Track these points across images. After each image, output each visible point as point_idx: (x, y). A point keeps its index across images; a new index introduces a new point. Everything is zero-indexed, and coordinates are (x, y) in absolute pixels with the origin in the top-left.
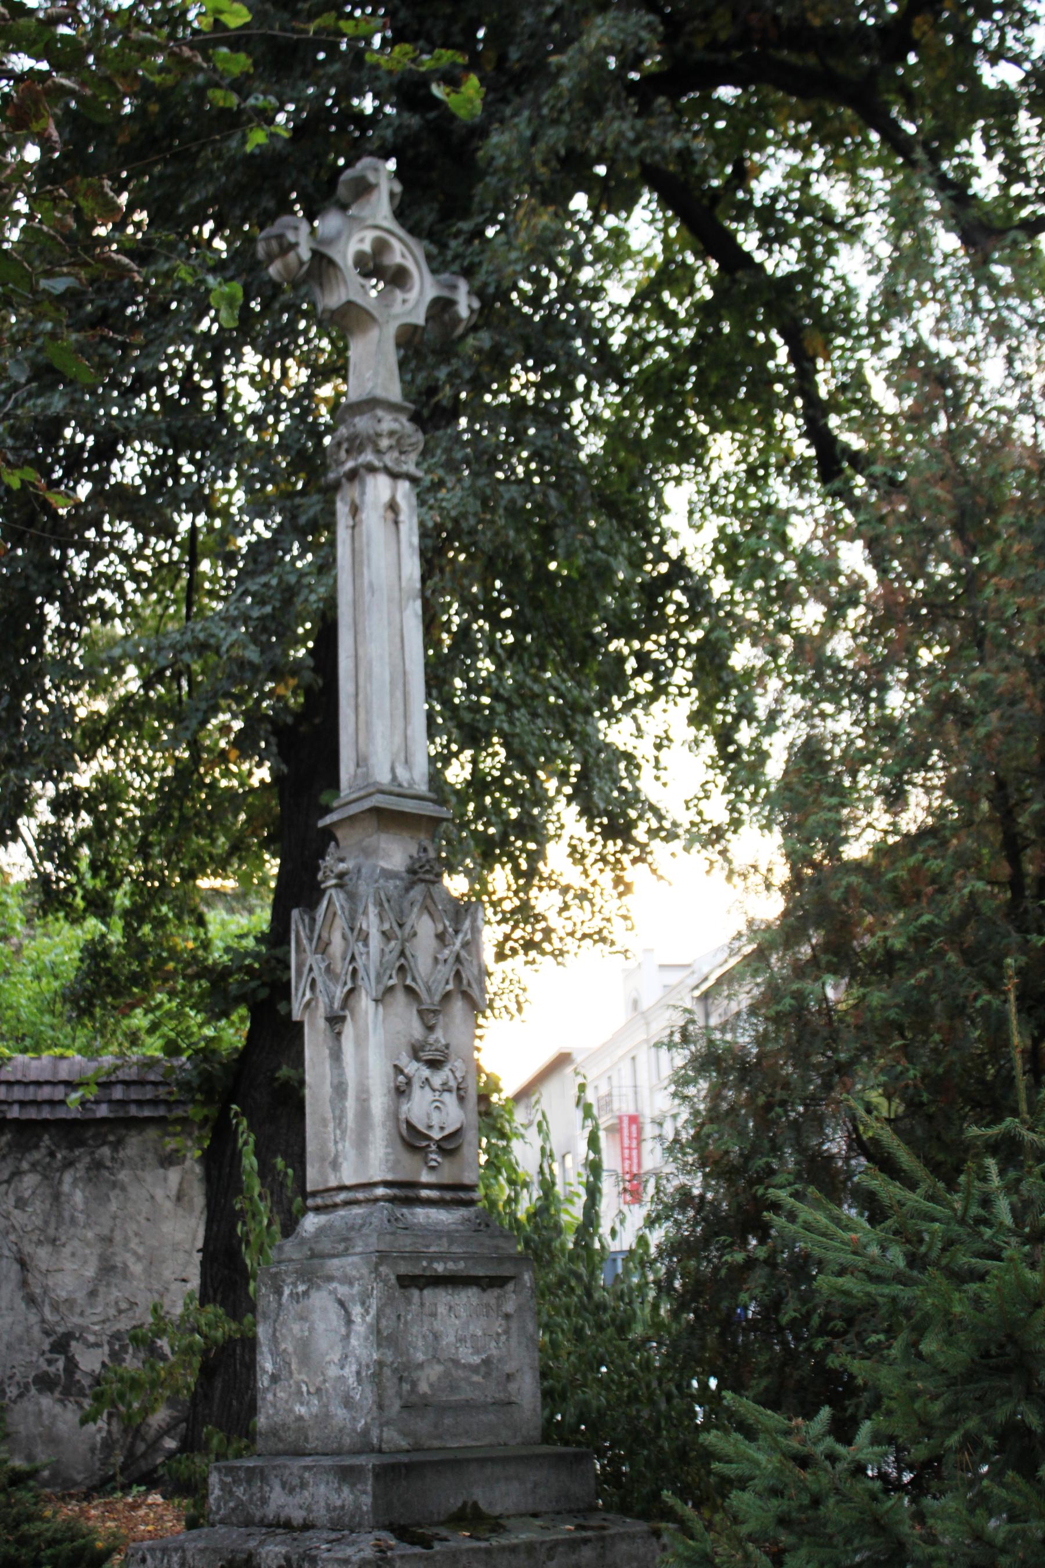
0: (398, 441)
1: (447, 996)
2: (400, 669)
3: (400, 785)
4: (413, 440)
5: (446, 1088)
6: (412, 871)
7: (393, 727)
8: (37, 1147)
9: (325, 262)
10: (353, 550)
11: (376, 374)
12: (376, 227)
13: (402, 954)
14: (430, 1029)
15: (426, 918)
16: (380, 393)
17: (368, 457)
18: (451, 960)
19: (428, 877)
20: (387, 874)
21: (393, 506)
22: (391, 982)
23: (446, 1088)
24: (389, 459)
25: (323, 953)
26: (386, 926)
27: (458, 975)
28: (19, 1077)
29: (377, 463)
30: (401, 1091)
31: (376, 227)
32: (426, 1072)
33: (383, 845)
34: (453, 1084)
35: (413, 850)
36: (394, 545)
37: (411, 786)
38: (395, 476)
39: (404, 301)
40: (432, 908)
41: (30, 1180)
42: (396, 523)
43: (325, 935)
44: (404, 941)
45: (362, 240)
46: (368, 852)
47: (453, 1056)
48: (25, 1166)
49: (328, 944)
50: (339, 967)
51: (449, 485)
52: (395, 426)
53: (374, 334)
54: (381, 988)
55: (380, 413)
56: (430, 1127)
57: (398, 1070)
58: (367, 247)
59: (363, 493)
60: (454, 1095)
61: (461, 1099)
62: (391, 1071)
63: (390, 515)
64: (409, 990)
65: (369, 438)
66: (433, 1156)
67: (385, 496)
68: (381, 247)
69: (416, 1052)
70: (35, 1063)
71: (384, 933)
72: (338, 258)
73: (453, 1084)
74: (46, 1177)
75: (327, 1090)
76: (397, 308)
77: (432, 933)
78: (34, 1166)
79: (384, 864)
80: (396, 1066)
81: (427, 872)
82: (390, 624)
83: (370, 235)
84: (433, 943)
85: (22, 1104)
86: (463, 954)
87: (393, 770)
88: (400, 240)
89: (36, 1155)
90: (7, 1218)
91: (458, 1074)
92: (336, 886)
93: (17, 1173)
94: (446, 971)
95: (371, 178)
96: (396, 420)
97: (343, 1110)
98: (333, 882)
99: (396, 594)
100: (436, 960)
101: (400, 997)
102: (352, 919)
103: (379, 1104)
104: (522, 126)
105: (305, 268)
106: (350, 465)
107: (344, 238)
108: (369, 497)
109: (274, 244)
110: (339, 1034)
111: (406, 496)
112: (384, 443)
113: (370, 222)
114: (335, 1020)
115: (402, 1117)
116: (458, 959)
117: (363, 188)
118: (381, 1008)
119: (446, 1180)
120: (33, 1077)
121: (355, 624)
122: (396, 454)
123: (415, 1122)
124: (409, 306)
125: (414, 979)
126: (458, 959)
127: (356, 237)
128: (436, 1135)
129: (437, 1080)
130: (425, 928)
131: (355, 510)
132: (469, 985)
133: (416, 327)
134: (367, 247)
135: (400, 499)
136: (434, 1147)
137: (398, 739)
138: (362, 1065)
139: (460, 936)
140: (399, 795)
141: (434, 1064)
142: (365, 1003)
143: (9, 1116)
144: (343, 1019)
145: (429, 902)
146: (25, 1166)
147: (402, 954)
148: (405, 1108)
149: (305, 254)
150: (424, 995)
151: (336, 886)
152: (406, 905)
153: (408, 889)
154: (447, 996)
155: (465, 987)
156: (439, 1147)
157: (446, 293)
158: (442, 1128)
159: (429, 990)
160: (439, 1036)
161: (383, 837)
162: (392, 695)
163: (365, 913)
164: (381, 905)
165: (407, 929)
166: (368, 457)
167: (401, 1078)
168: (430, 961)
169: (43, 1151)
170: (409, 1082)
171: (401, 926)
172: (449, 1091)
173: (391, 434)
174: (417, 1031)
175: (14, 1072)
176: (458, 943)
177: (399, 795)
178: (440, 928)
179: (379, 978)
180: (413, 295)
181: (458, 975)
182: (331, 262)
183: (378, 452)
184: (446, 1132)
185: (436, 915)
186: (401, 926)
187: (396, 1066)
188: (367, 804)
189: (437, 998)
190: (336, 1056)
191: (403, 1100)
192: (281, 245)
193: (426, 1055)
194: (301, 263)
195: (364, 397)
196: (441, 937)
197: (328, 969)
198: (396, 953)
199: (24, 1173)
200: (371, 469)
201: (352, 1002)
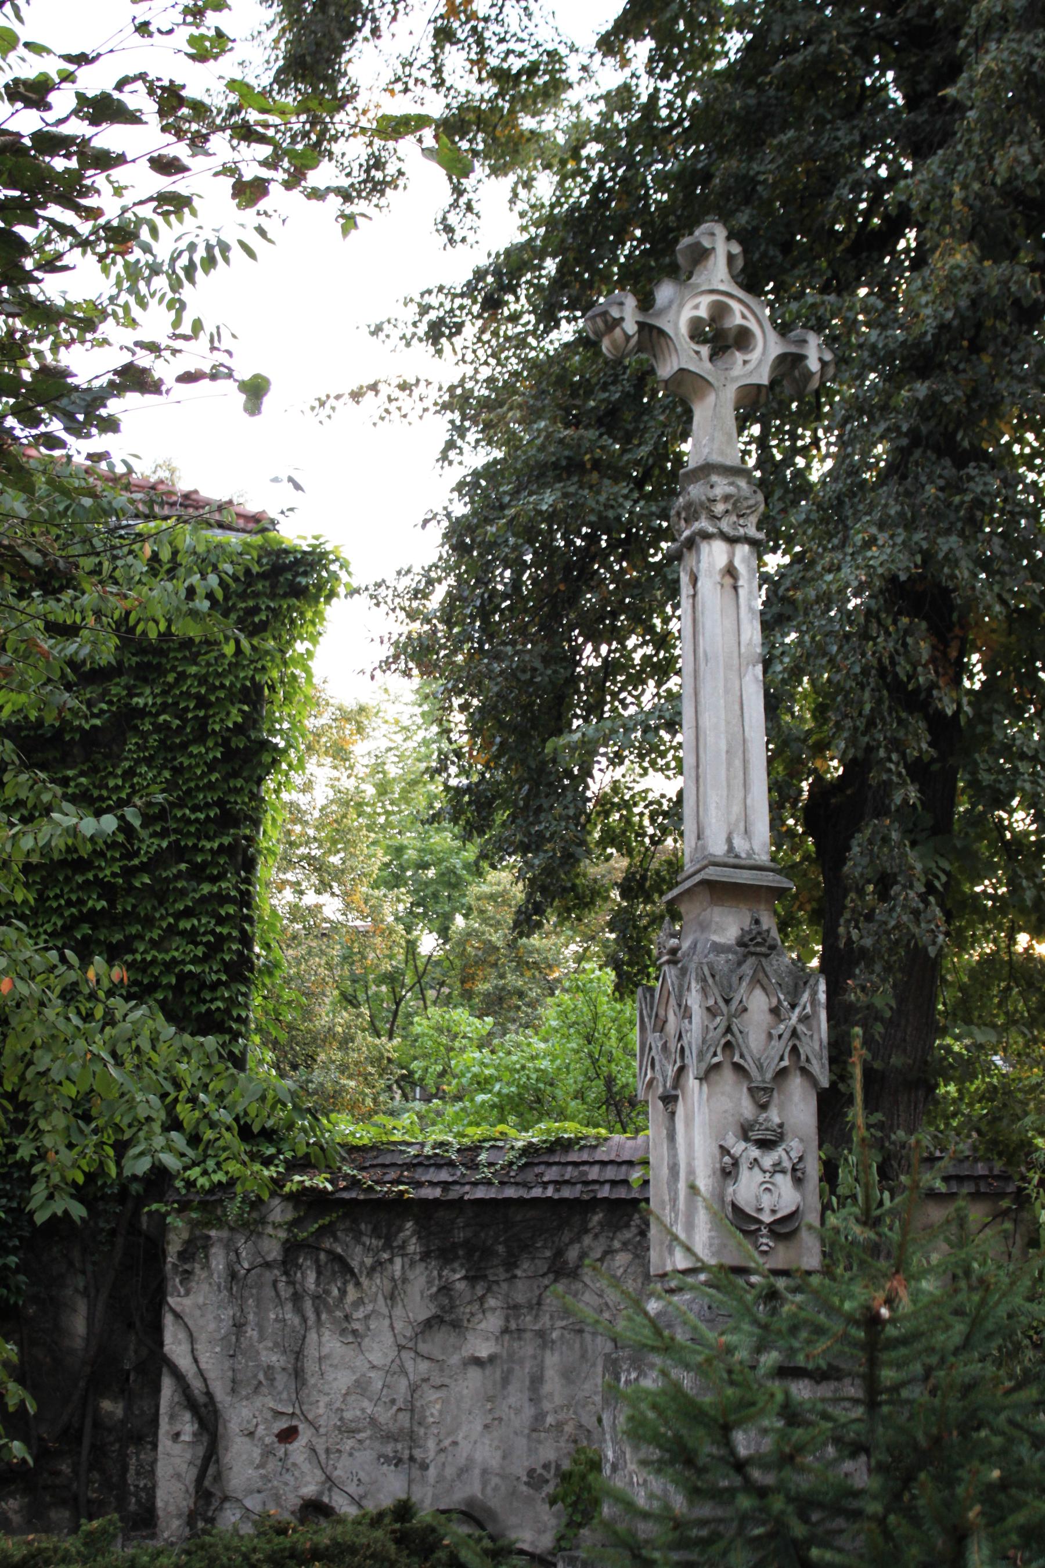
0: (734, 504)
1: (782, 1074)
2: (740, 737)
3: (737, 856)
4: (751, 502)
5: (778, 1168)
6: (741, 943)
7: (729, 797)
8: (627, 1226)
9: (655, 333)
10: (695, 621)
11: (712, 439)
12: (712, 292)
13: (729, 1030)
14: (764, 1107)
15: (758, 992)
16: (716, 458)
17: (703, 524)
18: (786, 1036)
19: (758, 949)
20: (718, 948)
21: (730, 571)
22: (716, 1060)
23: (778, 1168)
24: (725, 525)
25: (662, 1030)
26: (711, 1002)
27: (795, 1050)
28: (613, 1157)
29: (711, 530)
30: (728, 1172)
31: (712, 292)
32: (755, 1152)
33: (717, 919)
34: (787, 1164)
35: (747, 922)
36: (732, 611)
37: (749, 856)
38: (732, 540)
39: (745, 362)
40: (765, 981)
41: (622, 1259)
42: (735, 588)
43: (662, 1013)
44: (731, 1016)
45: (696, 307)
46: (704, 927)
47: (789, 1136)
48: (617, 1244)
49: (665, 1022)
50: (673, 1045)
51: (880, 542)
52: (731, 490)
53: (711, 398)
54: (704, 1066)
55: (714, 478)
56: (760, 1210)
57: (724, 1150)
58: (703, 313)
59: (698, 561)
60: (789, 1177)
61: (798, 1182)
62: (717, 1152)
63: (728, 580)
64: (738, 1068)
65: (702, 504)
66: (764, 1240)
67: (721, 561)
68: (719, 311)
69: (745, 1132)
70: (630, 1143)
71: (708, 1009)
72: (668, 329)
73: (787, 1164)
74: (637, 1256)
75: (665, 1171)
76: (738, 370)
77: (765, 1007)
78: (625, 1244)
79: (716, 938)
80: (721, 1147)
81: (758, 944)
82: (727, 691)
83: (706, 300)
84: (768, 1018)
85: (614, 1183)
86: (801, 1028)
87: (729, 841)
88: (740, 301)
89: (627, 1235)
90: (601, 1296)
91: (793, 1154)
92: (668, 962)
93: (609, 1252)
94: (779, 1047)
95: (706, 243)
96: (731, 484)
97: (676, 1192)
98: (665, 958)
99: (736, 661)
100: (770, 1036)
101: (728, 1074)
102: (680, 997)
103: (704, 1183)
104: (934, 167)
105: (634, 341)
106: (687, 533)
107: (675, 307)
108: (704, 565)
109: (599, 321)
110: (673, 1114)
111: (745, 560)
112: (719, 508)
113: (704, 288)
114: (669, 1100)
115: (728, 1199)
116: (794, 1033)
117: (701, 254)
118: (705, 1087)
119: (780, 1265)
120: (626, 1157)
121: (696, 694)
122: (734, 518)
123: (742, 1203)
124: (750, 367)
125: (742, 1056)
126: (794, 1033)
127: (689, 305)
128: (767, 1218)
129: (768, 1160)
130: (758, 1003)
131: (694, 580)
132: (808, 1060)
133: (759, 387)
134: (703, 313)
135: (737, 563)
136: (765, 1231)
137: (737, 809)
138: (690, 1145)
139: (797, 1010)
140: (735, 866)
141: (765, 1145)
142: (692, 1083)
143: (600, 1196)
144: (676, 1098)
145: (761, 975)
146: (617, 1244)
147: (729, 1030)
148: (730, 1190)
149: (630, 327)
150: (754, 1072)
151: (668, 962)
152: (735, 980)
153: (740, 964)
154: (782, 1074)
155: (803, 1063)
156: (771, 1231)
157: (793, 349)
158: (773, 1212)
159: (760, 1068)
160: (774, 1116)
161: (717, 910)
162: (729, 764)
163: (689, 989)
164: (704, 980)
165: (734, 1004)
166: (703, 524)
167: (727, 1159)
168: (763, 1036)
169: (634, 1230)
170: (736, 1163)
171: (727, 1002)
172: (783, 1171)
173: (726, 498)
174: (747, 1109)
175: (608, 1152)
176: (795, 1016)
177: (735, 866)
178: (774, 1002)
179: (701, 1055)
180: (755, 356)
181: (795, 1050)
182: (661, 332)
183: (714, 518)
184: (779, 1215)
185: (770, 988)
186: (727, 1002)
187: (721, 1147)
188: (697, 878)
189: (769, 1075)
190: (672, 1137)
191: (730, 1182)
192: (606, 322)
193: (754, 1135)
194: (628, 338)
195: (701, 462)
196: (775, 1011)
197: (665, 1047)
198: (721, 1029)
199: (616, 1251)
200: (707, 536)
201: (682, 1081)
